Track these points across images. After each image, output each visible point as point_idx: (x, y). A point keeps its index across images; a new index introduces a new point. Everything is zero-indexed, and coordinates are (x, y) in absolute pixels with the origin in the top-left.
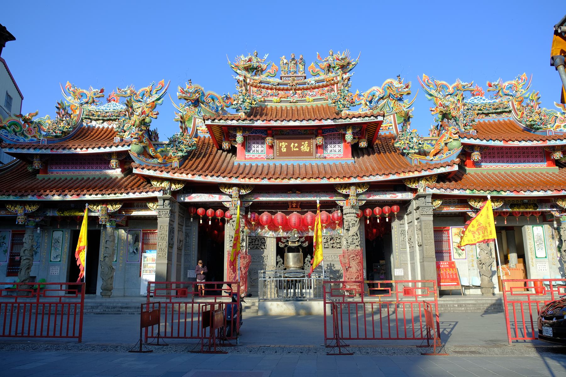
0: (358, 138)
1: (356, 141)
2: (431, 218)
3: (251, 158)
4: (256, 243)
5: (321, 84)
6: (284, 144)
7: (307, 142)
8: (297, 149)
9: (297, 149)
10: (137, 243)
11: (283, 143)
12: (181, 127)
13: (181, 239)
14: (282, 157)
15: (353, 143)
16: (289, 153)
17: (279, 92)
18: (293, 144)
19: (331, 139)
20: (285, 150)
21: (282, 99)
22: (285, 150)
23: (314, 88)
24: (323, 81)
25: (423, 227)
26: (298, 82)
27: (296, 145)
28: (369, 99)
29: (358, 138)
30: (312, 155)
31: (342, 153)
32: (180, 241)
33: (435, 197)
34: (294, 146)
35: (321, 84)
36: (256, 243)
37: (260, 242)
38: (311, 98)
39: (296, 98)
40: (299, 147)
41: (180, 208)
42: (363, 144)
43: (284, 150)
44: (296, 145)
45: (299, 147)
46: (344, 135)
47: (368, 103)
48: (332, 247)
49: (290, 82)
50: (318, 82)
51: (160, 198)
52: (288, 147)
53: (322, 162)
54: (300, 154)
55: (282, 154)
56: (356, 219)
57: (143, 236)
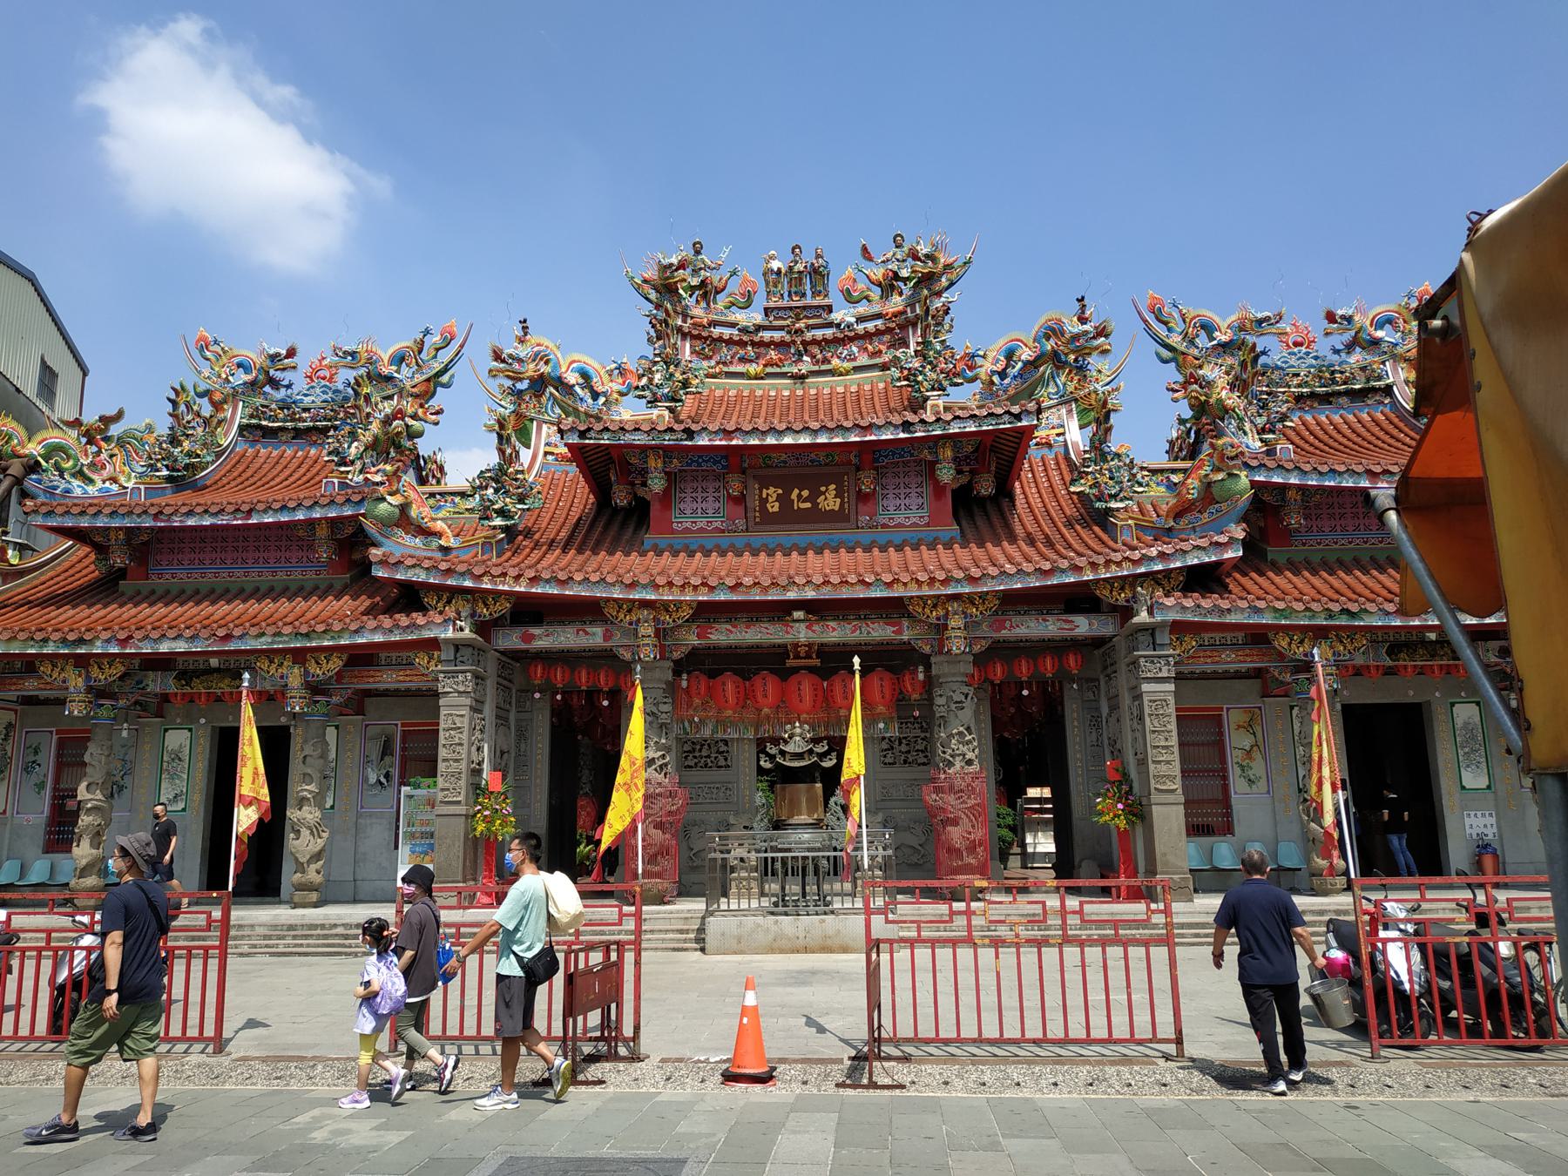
0: (971, 471)
1: (964, 479)
2: (1172, 687)
3: (687, 530)
4: (704, 753)
5: (870, 326)
6: (772, 492)
7: (833, 487)
8: (808, 505)
9: (808, 505)
10: (387, 759)
11: (772, 489)
12: (501, 452)
13: (505, 748)
14: (768, 527)
15: (955, 486)
16: (788, 517)
17: (762, 350)
18: (796, 491)
19: (897, 475)
20: (776, 509)
21: (769, 370)
22: (776, 509)
23: (851, 339)
24: (878, 316)
25: (1147, 711)
26: (811, 322)
27: (805, 493)
28: (999, 367)
29: (971, 471)
30: (846, 519)
31: (925, 513)
32: (502, 753)
33: (1178, 628)
34: (799, 496)
35: (870, 326)
36: (704, 753)
37: (714, 749)
38: (848, 365)
39: (806, 365)
40: (812, 498)
41: (503, 666)
42: (986, 488)
43: (774, 507)
44: (805, 493)
45: (812, 498)
46: (932, 466)
47: (996, 379)
48: (905, 762)
49: (788, 322)
50: (860, 319)
51: (447, 641)
52: (784, 500)
53: (715, 541)
54: (816, 517)
55: (768, 519)
56: (965, 689)
57: (404, 740)
